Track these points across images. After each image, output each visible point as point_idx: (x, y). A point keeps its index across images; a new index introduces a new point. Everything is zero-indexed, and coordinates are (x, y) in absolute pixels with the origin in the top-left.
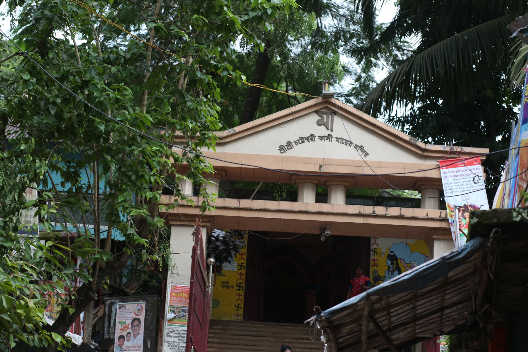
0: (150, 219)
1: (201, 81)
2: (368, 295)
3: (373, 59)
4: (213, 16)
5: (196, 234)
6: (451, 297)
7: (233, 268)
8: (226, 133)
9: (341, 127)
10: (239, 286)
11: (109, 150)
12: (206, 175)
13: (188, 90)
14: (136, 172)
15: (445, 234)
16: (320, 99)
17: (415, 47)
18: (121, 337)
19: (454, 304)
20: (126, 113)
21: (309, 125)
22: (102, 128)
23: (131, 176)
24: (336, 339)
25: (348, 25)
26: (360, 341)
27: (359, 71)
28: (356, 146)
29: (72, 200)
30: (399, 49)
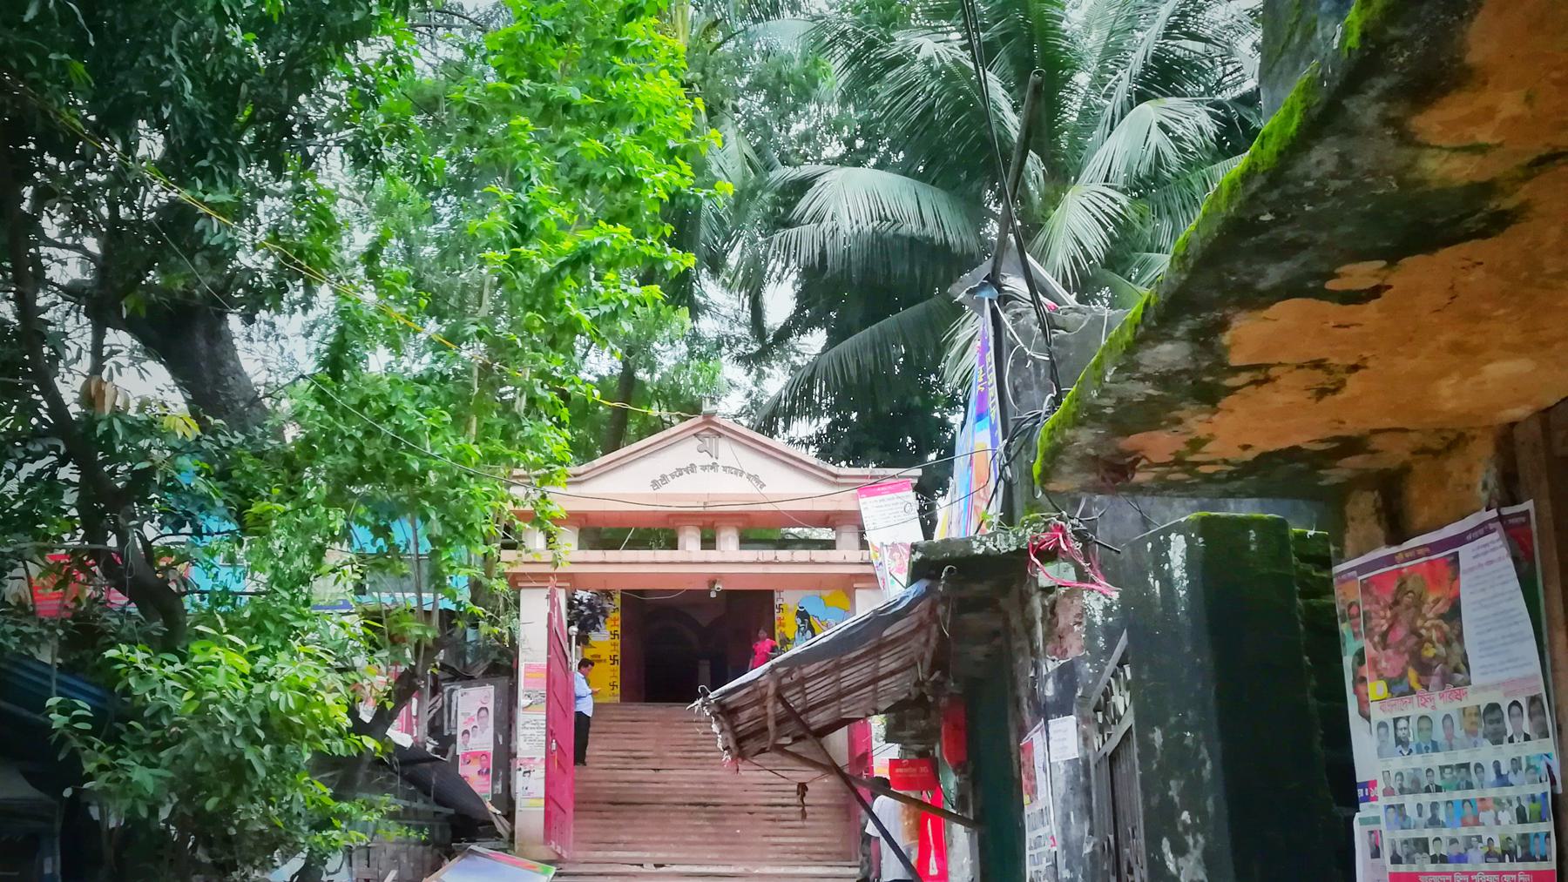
0: (485, 581)
1: (542, 399)
2: (773, 668)
3: (765, 369)
4: (553, 314)
5: (551, 597)
6: (888, 663)
7: (605, 640)
8: (583, 468)
9: (727, 452)
10: (613, 660)
11: (426, 495)
12: (557, 521)
13: (527, 412)
14: (463, 521)
15: (870, 579)
16: (700, 419)
17: (818, 350)
18: (466, 732)
19: (892, 673)
20: (442, 446)
21: (687, 452)
22: (416, 466)
23: (458, 528)
24: (733, 728)
25: (731, 328)
26: (766, 729)
27: (749, 385)
28: (749, 476)
29: (382, 561)
30: (798, 353)
